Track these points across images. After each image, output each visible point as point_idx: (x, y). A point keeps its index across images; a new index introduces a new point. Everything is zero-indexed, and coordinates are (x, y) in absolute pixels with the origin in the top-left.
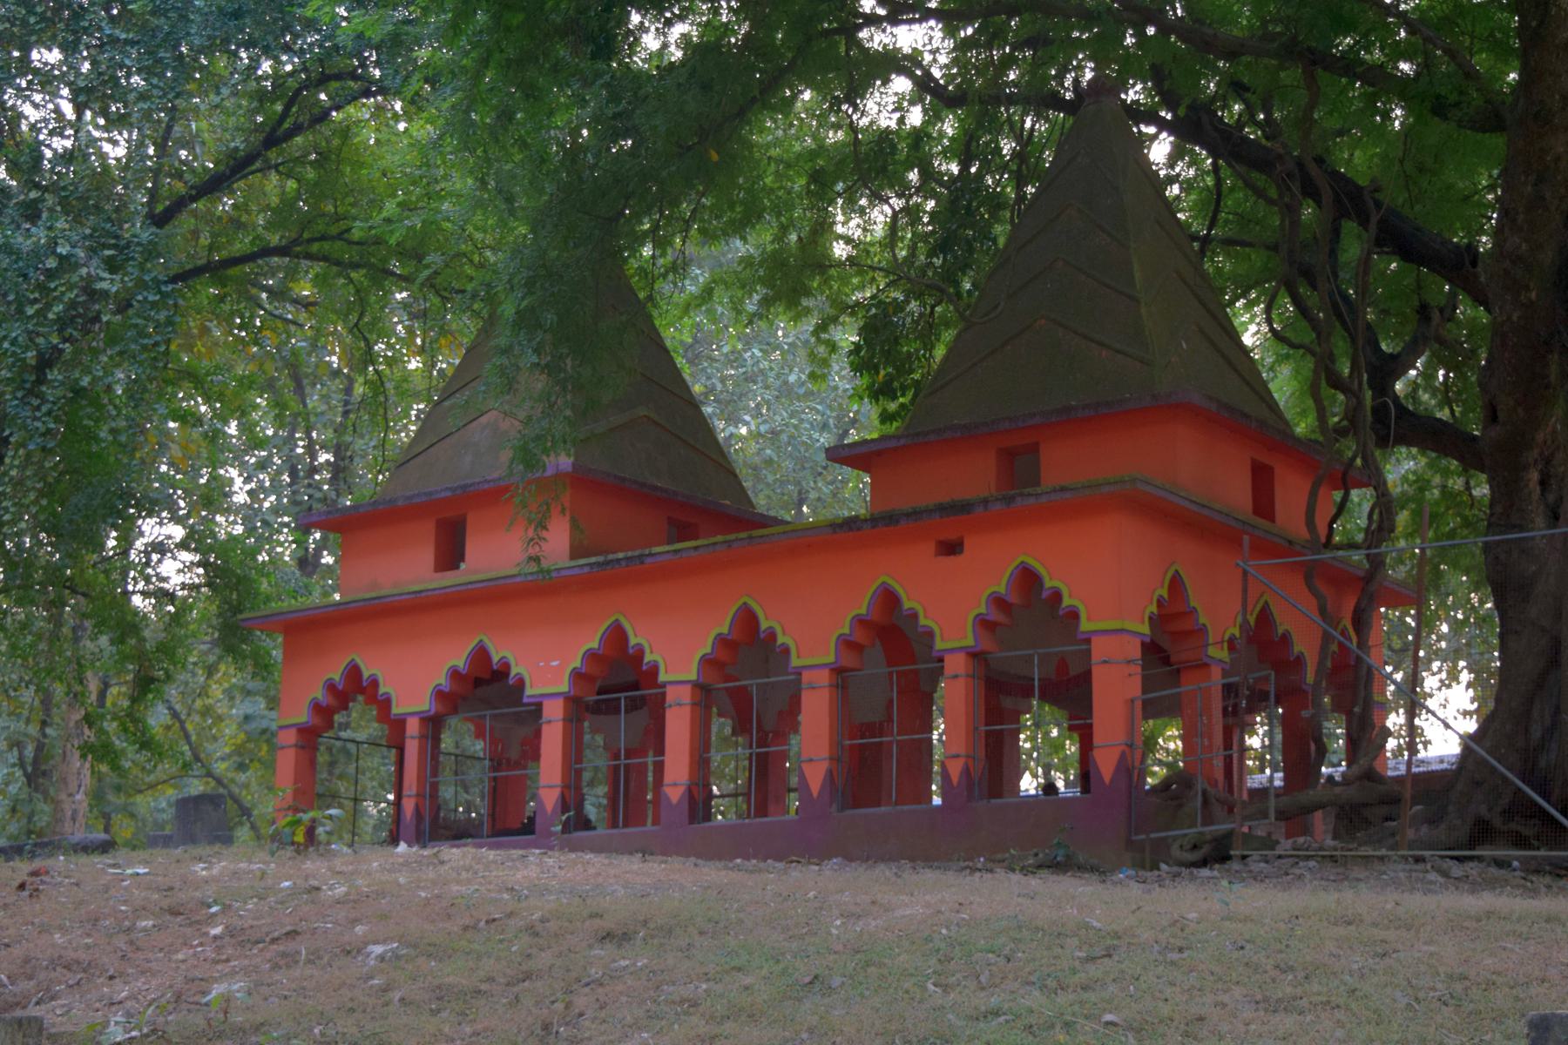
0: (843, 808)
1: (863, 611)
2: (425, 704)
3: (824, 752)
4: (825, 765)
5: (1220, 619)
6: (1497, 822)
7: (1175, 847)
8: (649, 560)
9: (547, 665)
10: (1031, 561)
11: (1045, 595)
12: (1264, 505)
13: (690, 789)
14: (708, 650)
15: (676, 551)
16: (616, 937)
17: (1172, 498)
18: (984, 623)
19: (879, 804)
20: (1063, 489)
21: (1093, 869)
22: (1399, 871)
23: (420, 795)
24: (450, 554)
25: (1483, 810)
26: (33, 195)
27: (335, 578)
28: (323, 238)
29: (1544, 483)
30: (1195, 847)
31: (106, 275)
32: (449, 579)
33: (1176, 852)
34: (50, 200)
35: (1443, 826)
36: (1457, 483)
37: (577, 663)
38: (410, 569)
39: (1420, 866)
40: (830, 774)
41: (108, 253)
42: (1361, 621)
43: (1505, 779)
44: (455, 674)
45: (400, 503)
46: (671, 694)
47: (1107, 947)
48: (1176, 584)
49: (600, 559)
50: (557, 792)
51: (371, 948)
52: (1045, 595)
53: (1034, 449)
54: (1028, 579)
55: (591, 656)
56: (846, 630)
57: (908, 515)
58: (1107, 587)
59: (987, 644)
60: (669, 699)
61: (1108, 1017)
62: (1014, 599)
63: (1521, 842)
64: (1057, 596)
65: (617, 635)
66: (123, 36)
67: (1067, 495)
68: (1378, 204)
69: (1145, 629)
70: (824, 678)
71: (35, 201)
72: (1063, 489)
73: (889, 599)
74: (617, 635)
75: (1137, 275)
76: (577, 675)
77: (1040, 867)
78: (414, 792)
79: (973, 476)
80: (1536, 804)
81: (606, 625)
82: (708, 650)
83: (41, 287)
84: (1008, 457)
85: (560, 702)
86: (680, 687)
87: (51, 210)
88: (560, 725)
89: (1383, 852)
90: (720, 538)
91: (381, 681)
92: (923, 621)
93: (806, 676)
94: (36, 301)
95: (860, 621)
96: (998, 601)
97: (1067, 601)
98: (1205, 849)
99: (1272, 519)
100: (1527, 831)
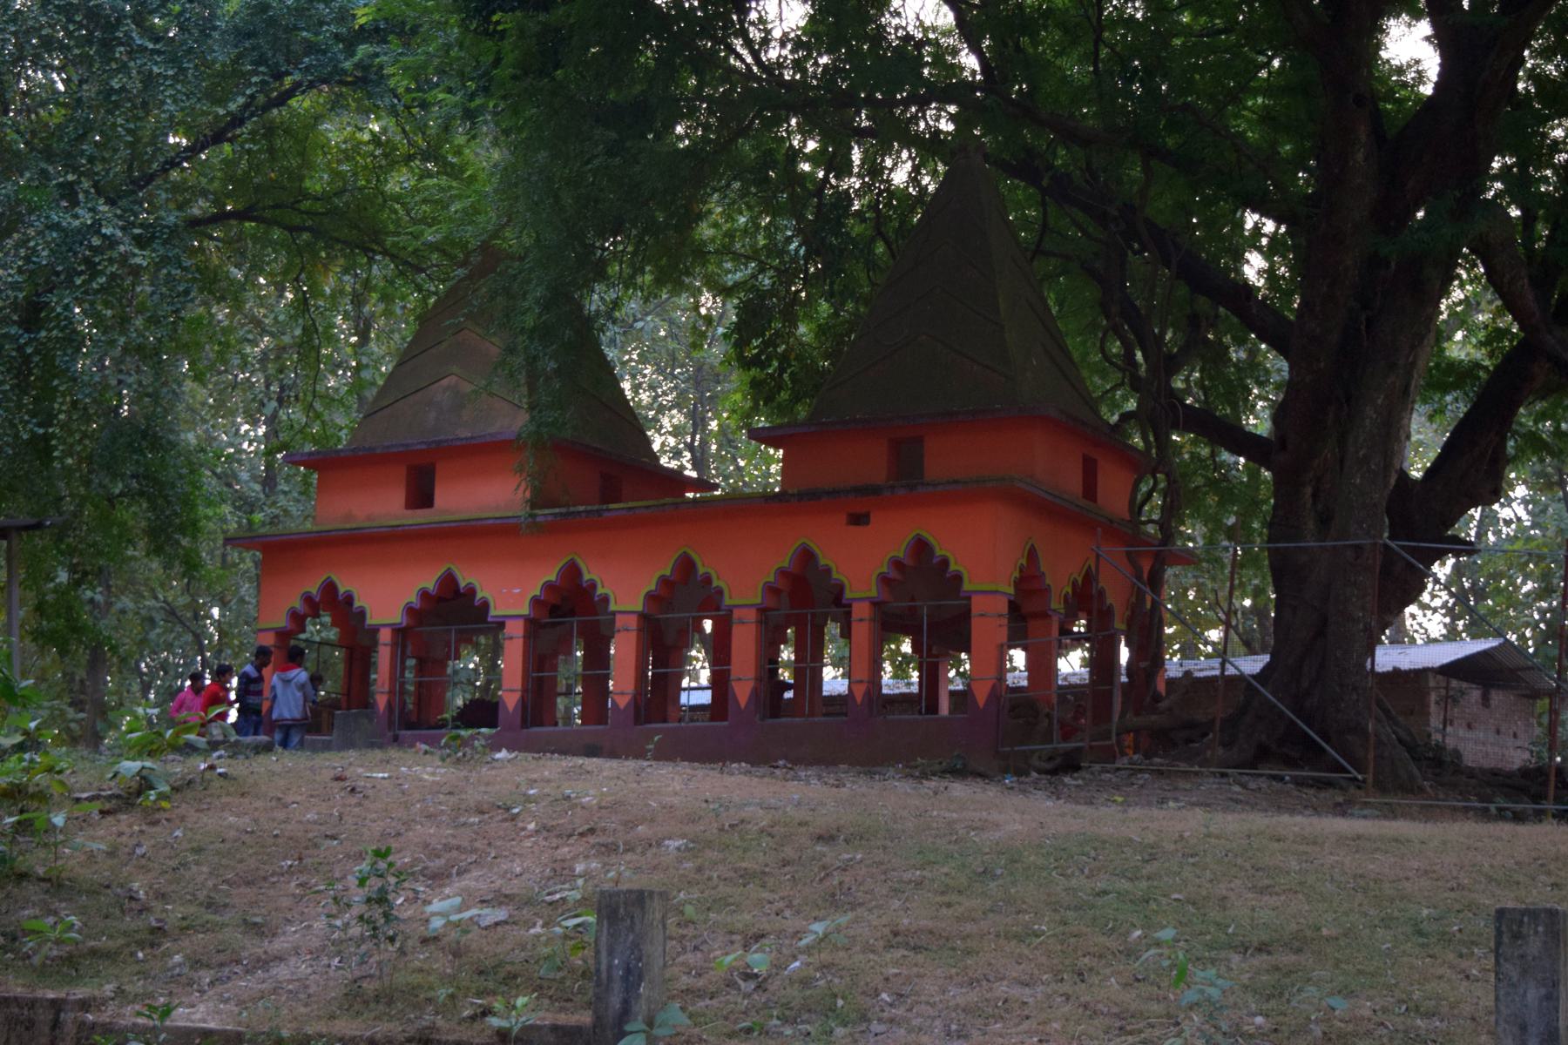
1: (786, 564)
2: (397, 617)
3: (751, 674)
4: (752, 684)
5: (1060, 579)
8: (606, 514)
9: (510, 591)
10: (925, 534)
12: (1090, 491)
14: (653, 587)
16: (827, 838)
18: (884, 580)
21: (982, 776)
22: (1210, 784)
23: (391, 692)
24: (421, 497)
26: (70, 177)
27: (298, 508)
29: (1315, 496)
30: (1050, 759)
32: (420, 517)
33: (1035, 761)
34: (86, 184)
36: (1205, 452)
37: (538, 593)
38: (385, 506)
42: (1155, 581)
44: (424, 594)
47: (1152, 853)
48: (1032, 555)
49: (564, 510)
50: (518, 695)
54: (921, 547)
57: (828, 493)
58: (983, 555)
60: (618, 625)
61: (1176, 896)
62: (909, 562)
63: (1291, 763)
64: (945, 562)
65: (572, 571)
66: (151, 46)
69: (1011, 590)
70: (751, 615)
71: (71, 184)
72: (956, 482)
73: (806, 556)
76: (535, 602)
77: (944, 772)
78: (386, 689)
79: (868, 462)
80: (1314, 741)
83: (87, 261)
85: (520, 623)
86: (626, 617)
87: (86, 192)
89: (1196, 768)
90: (668, 500)
91: (356, 597)
92: (835, 575)
93: (736, 614)
94: (82, 273)
96: (897, 564)
97: (953, 567)
98: (1058, 760)
99: (1094, 500)
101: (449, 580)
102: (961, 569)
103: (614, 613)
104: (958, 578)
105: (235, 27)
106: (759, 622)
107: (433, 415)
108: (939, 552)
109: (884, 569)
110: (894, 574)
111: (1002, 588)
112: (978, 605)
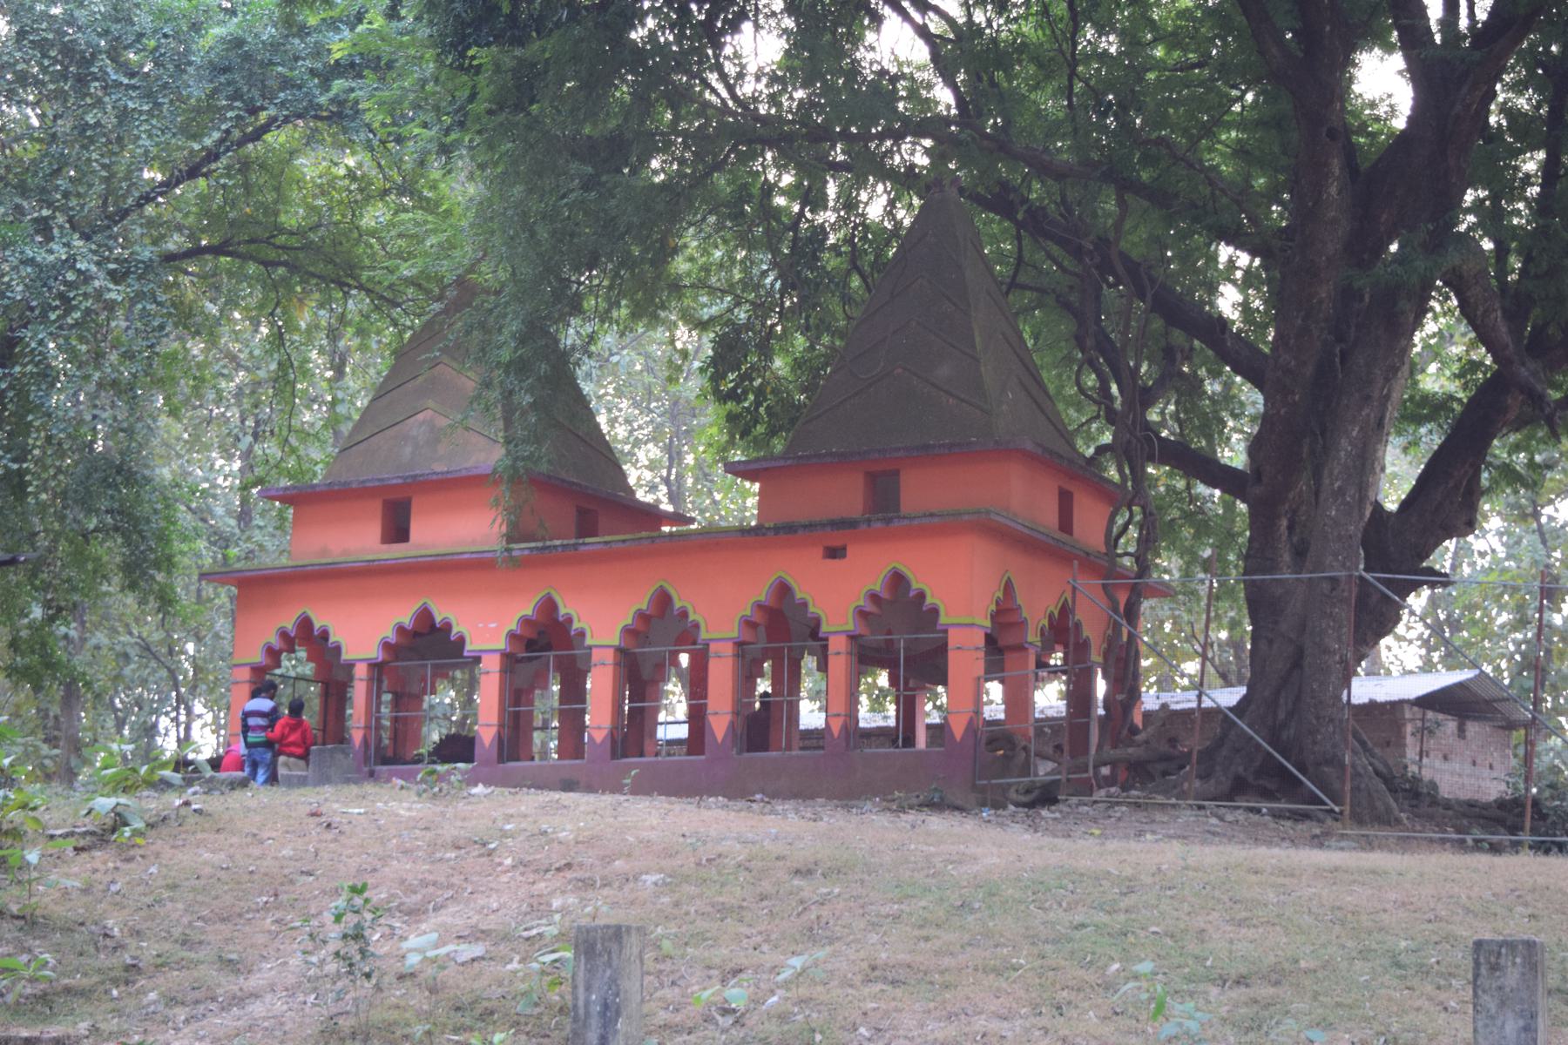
0: (740, 752)
2: (374, 653)
5: (1036, 611)
6: (1251, 779)
7: (1013, 790)
8: (582, 548)
9: (486, 626)
10: (898, 566)
11: (912, 594)
12: (1066, 524)
13: (612, 734)
14: (629, 621)
15: (606, 543)
16: (803, 872)
17: (1013, 524)
19: (766, 750)
20: (932, 515)
22: (1187, 816)
24: (397, 531)
25: (1241, 769)
26: (45, 213)
28: (252, 241)
29: (1291, 528)
30: (1028, 792)
31: (111, 286)
32: (397, 552)
33: (1013, 795)
34: (61, 219)
35: (1212, 781)
36: (1180, 484)
37: (513, 626)
39: (1202, 812)
40: (732, 725)
41: (112, 266)
42: (1131, 614)
43: (1258, 746)
44: (401, 629)
45: (354, 486)
46: (596, 656)
48: (1008, 588)
49: (540, 544)
50: (493, 731)
51: (644, 877)
52: (912, 594)
53: (897, 473)
55: (525, 621)
56: (748, 612)
57: (805, 527)
58: (960, 588)
59: (861, 630)
60: (594, 659)
61: (1154, 929)
62: (885, 595)
63: (1267, 795)
65: (549, 606)
67: (936, 520)
68: (1152, 281)
69: (988, 623)
70: (728, 649)
71: (46, 219)
72: (932, 515)
73: (783, 589)
74: (549, 606)
75: (978, 340)
76: (512, 636)
77: (920, 805)
78: (362, 724)
79: (844, 495)
81: (536, 600)
82: (629, 621)
83: (62, 296)
84: (872, 478)
85: (497, 658)
87: (61, 227)
88: (497, 676)
89: (1173, 801)
90: (644, 534)
92: (812, 609)
93: (713, 647)
94: (57, 307)
95: (759, 606)
96: (874, 597)
97: (929, 600)
100: (1271, 786)
101: (425, 615)
102: (937, 601)
103: (590, 648)
104: (935, 611)
105: (210, 62)
106: (736, 656)
107: (408, 450)
108: (915, 585)
109: (862, 603)
110: (870, 608)
111: (979, 621)
112: (954, 639)
